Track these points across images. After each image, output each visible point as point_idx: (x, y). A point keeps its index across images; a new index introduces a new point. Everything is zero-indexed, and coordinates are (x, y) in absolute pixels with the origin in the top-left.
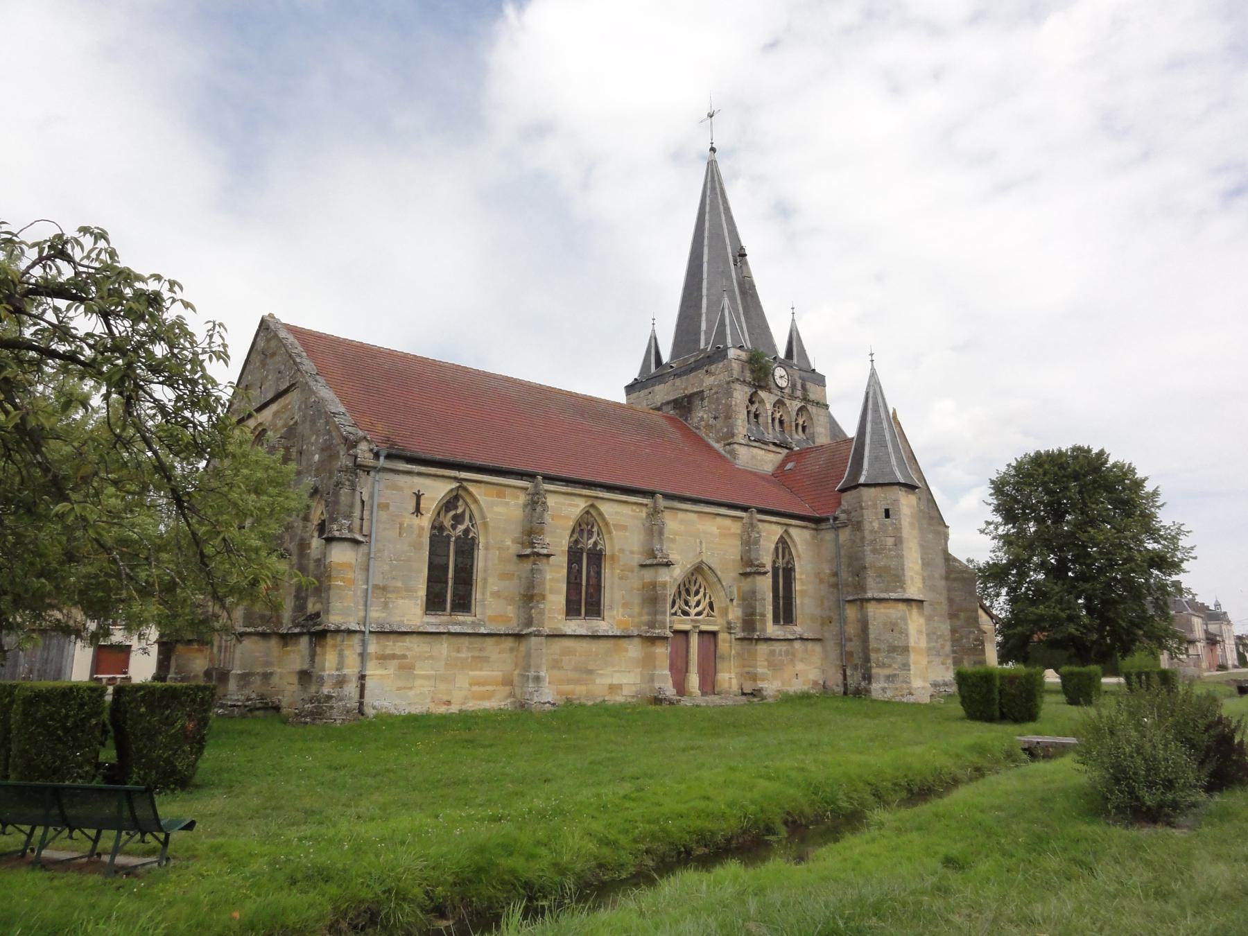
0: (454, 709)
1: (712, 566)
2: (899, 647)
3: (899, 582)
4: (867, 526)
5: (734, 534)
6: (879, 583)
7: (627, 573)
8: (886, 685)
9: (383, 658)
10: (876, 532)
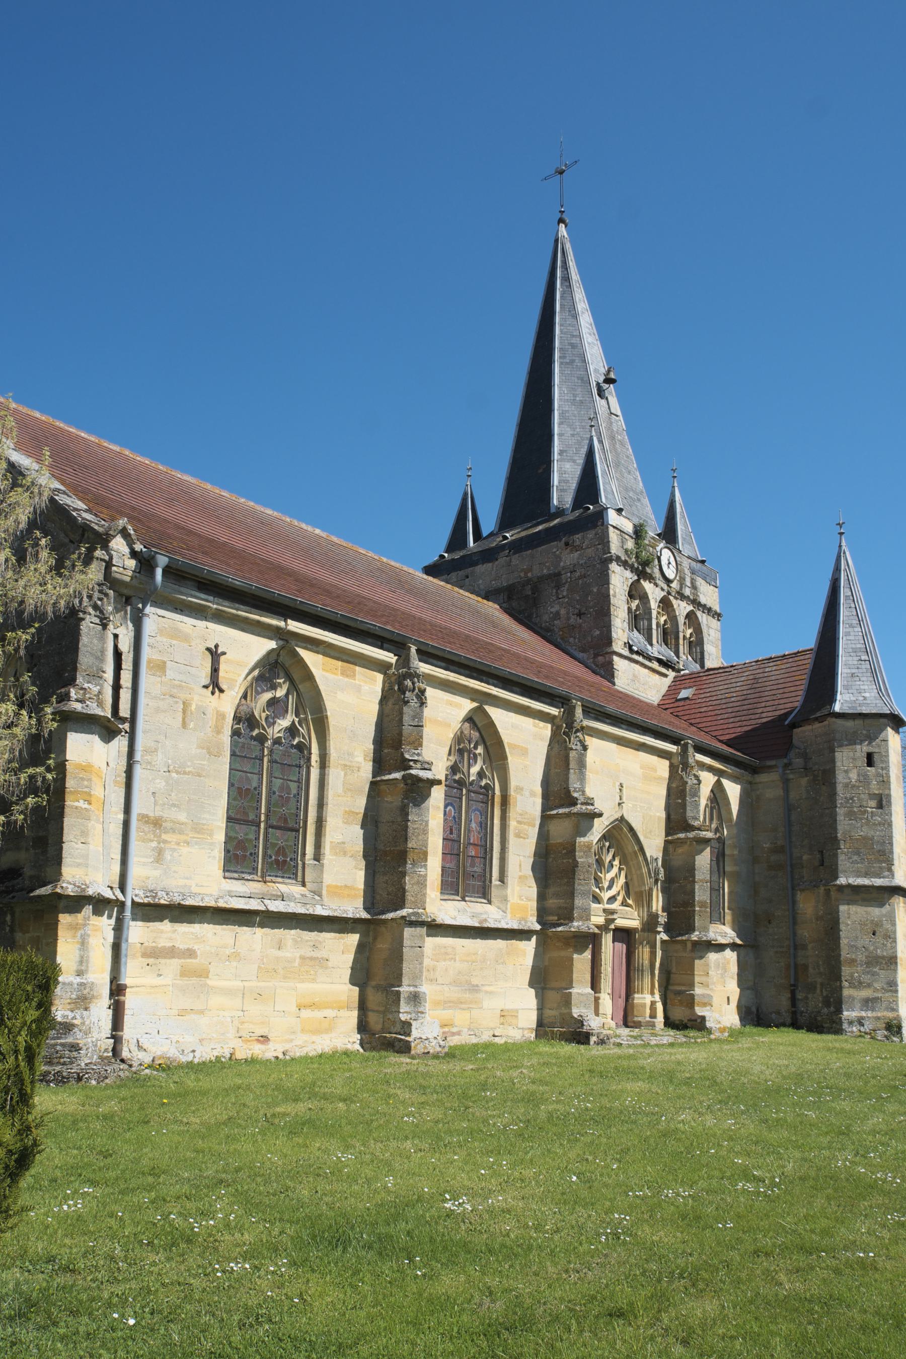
0: (270, 1052)
1: (634, 825)
2: (883, 957)
3: (885, 862)
4: (840, 778)
5: (661, 778)
6: (856, 862)
7: (526, 827)
8: (863, 1014)
9: (153, 953)
10: (854, 786)
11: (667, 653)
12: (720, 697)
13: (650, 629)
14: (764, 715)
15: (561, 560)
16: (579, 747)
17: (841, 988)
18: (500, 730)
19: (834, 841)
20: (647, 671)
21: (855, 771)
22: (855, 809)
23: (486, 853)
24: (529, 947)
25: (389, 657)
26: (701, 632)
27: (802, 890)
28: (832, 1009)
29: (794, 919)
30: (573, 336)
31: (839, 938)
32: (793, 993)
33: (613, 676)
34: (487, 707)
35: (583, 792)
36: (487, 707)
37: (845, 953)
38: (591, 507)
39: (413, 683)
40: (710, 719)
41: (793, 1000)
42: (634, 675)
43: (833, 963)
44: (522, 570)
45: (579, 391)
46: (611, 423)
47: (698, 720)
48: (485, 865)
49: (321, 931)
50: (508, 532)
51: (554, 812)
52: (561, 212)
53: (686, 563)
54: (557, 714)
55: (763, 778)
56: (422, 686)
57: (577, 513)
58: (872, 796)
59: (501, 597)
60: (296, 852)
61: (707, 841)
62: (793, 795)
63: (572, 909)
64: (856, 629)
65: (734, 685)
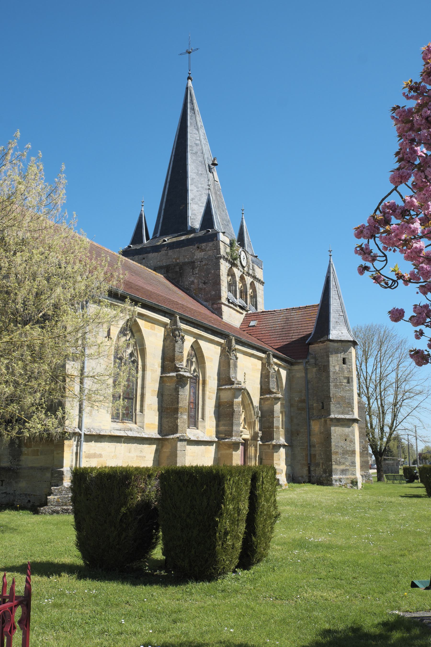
2: (350, 451)
3: (350, 407)
4: (332, 369)
8: (341, 477)
10: (337, 373)
11: (243, 303)
12: (271, 326)
13: (236, 291)
14: (293, 337)
15: (195, 255)
16: (234, 358)
17: (332, 465)
18: (203, 350)
19: (329, 398)
20: (235, 311)
21: (338, 366)
22: (338, 384)
23: (196, 406)
24: (212, 449)
25: (167, 320)
26: (256, 292)
27: (313, 420)
28: (327, 474)
29: (309, 433)
30: (196, 140)
31: (331, 442)
32: (309, 468)
33: (222, 315)
34: (198, 340)
35: (236, 378)
36: (198, 340)
37: (333, 449)
38: (210, 230)
39: (179, 333)
40: (267, 337)
41: (309, 471)
42: (230, 314)
43: (328, 453)
44: (174, 258)
45: (200, 168)
46: (215, 185)
47: (261, 338)
48: (195, 412)
49: (143, 444)
50: (166, 238)
51: (223, 387)
52: (189, 73)
53: (250, 257)
54: (223, 342)
55: (296, 367)
56: (183, 334)
57: (203, 232)
58: (345, 378)
59: (163, 271)
60: (132, 409)
61: (279, 399)
62: (309, 376)
63: (232, 431)
64: (338, 301)
65: (277, 321)
